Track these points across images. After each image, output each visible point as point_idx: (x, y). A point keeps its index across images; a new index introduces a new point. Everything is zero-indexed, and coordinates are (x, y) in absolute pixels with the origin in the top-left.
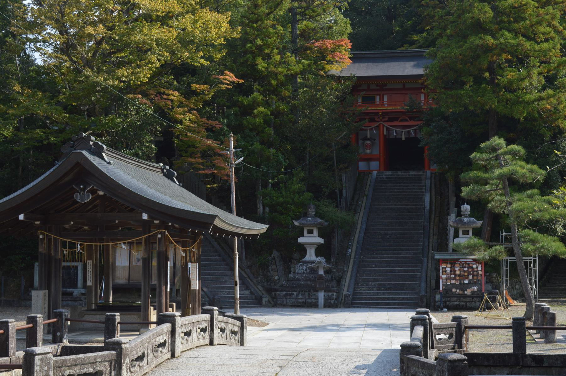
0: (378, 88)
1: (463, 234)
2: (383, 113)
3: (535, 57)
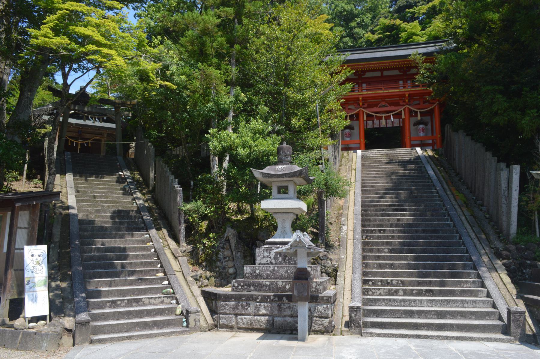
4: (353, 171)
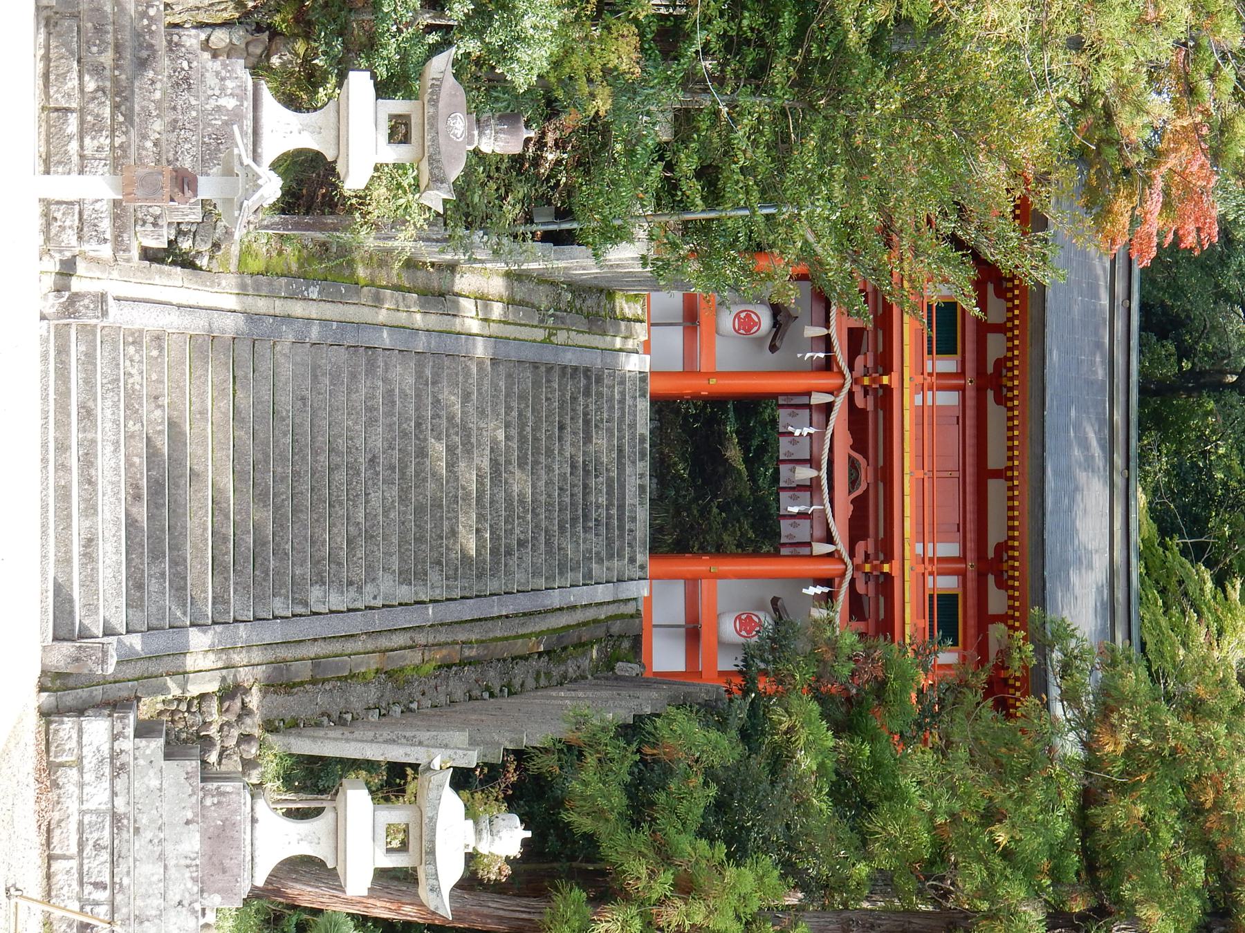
0: (990, 369)
1: (390, 830)
2: (888, 390)
3: (307, 61)
4: (540, 334)
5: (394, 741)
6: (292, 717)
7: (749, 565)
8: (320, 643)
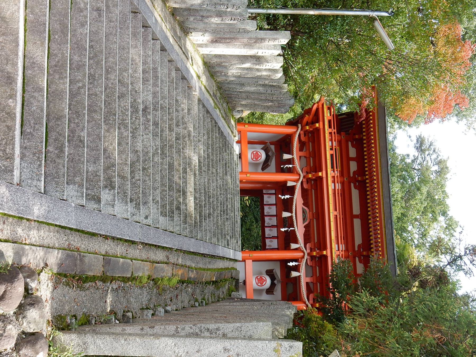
5: (197, 334)
6: (84, 314)
7: (265, 253)
8: (109, 242)
